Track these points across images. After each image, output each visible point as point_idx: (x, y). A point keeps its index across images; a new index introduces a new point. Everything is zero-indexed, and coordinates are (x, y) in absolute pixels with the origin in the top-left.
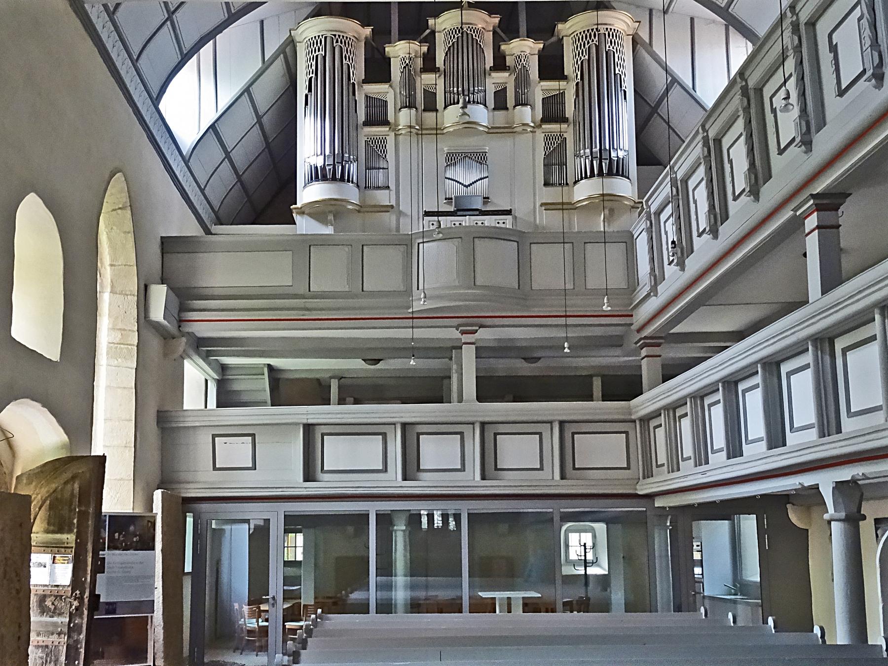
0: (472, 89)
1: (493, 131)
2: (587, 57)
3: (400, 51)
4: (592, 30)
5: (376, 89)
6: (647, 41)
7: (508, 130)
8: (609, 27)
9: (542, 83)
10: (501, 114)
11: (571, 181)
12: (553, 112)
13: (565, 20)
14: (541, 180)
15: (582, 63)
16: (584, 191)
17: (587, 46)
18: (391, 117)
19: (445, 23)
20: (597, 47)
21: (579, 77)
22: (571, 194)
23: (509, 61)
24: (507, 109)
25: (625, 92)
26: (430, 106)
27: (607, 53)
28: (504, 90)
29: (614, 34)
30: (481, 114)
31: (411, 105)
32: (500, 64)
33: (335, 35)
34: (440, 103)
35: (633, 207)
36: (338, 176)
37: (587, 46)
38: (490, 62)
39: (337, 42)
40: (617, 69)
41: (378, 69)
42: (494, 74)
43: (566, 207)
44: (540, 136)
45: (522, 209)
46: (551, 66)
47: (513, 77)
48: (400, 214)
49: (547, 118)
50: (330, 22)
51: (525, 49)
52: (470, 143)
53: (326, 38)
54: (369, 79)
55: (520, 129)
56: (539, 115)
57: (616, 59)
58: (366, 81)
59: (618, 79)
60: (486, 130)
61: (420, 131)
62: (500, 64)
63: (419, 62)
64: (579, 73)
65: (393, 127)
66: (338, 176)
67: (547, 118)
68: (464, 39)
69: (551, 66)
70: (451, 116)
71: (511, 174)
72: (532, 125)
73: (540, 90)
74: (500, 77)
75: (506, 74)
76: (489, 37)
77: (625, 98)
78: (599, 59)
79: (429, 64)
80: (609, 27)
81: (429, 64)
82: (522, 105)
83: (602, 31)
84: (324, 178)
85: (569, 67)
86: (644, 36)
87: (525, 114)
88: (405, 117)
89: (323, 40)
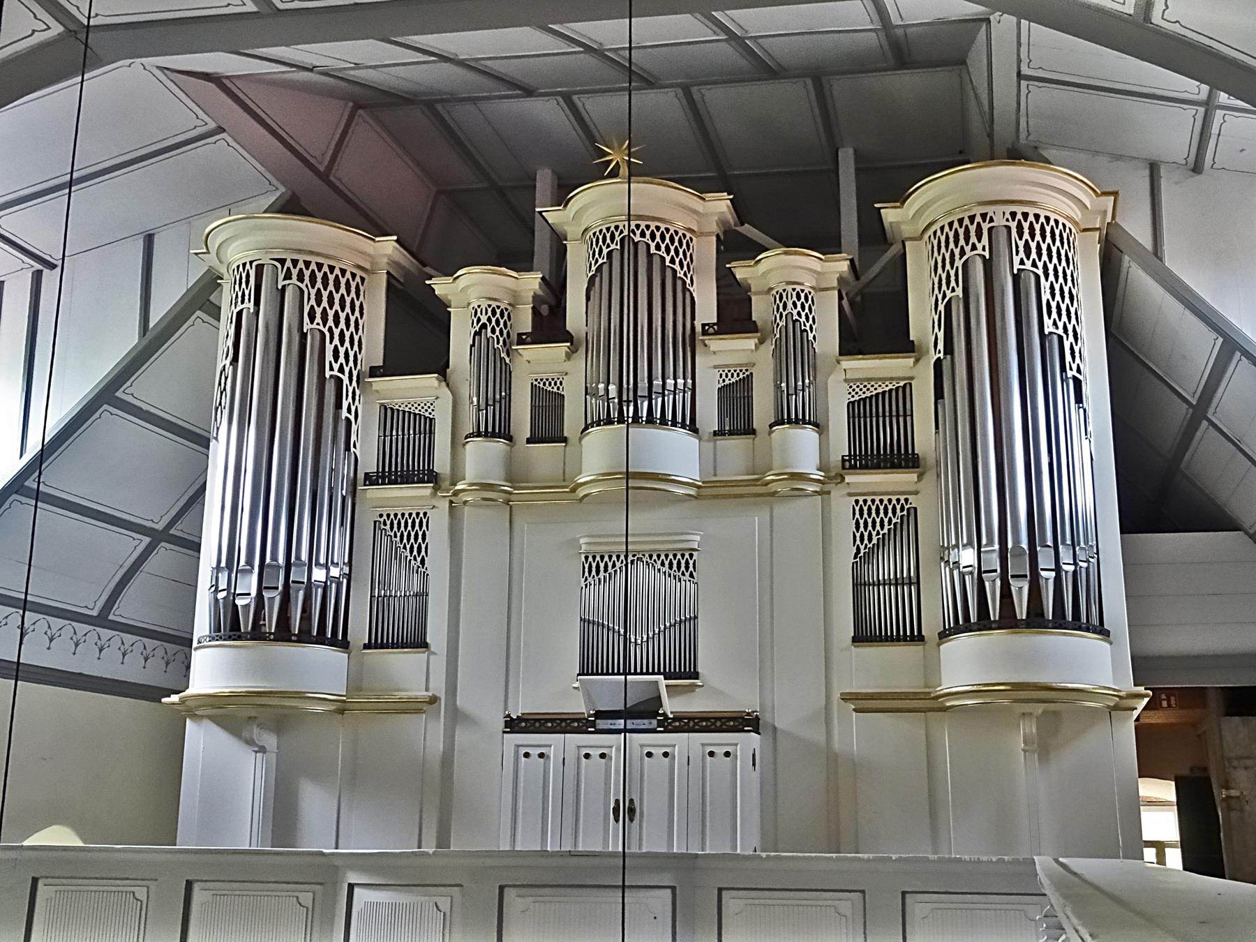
0: (657, 382)
1: (711, 492)
2: (959, 292)
3: (468, 291)
4: (608, 229)
5: (414, 390)
6: (1148, 245)
7: (755, 489)
8: (1019, 210)
9: (850, 364)
10: (734, 447)
11: (930, 627)
12: (879, 441)
13: (899, 196)
14: (845, 626)
15: (948, 307)
16: (966, 663)
17: (959, 263)
18: (441, 462)
19: (590, 210)
20: (988, 265)
21: (941, 346)
22: (931, 668)
23: (760, 309)
24: (753, 432)
25: (1078, 383)
26: (548, 428)
27: (1016, 278)
28: (747, 381)
29: (1034, 227)
30: (677, 454)
31: (500, 430)
32: (735, 314)
33: (282, 261)
34: (571, 425)
35: (1116, 708)
36: (1022, 612)
37: (959, 263)
38: (707, 311)
39: (288, 276)
40: (1048, 323)
41: (418, 336)
42: (715, 344)
43: (926, 703)
44: (842, 506)
45: (788, 713)
46: (875, 321)
47: (769, 347)
48: (456, 716)
49: (864, 458)
50: (285, 228)
51: (802, 279)
52: (650, 525)
53: (260, 269)
54: (398, 361)
55: (782, 488)
56: (840, 445)
57: (1046, 296)
58: (388, 368)
59: (1056, 354)
60: (692, 492)
61: (510, 491)
62: (735, 314)
63: (525, 322)
64: (941, 335)
65: (446, 484)
66: (1022, 612)
67: (864, 458)
68: (634, 257)
69: (875, 321)
70: (596, 452)
71: (769, 605)
72: (818, 475)
73: (844, 380)
74: (738, 348)
75: (749, 343)
76: (706, 251)
77: (1079, 399)
78: (998, 299)
79: (550, 324)
80: (1019, 210)
81: (550, 324)
82: (797, 422)
83: (999, 221)
84: (985, 623)
85: (922, 320)
86: (1137, 228)
87: (802, 449)
88: (482, 458)
89: (252, 273)
